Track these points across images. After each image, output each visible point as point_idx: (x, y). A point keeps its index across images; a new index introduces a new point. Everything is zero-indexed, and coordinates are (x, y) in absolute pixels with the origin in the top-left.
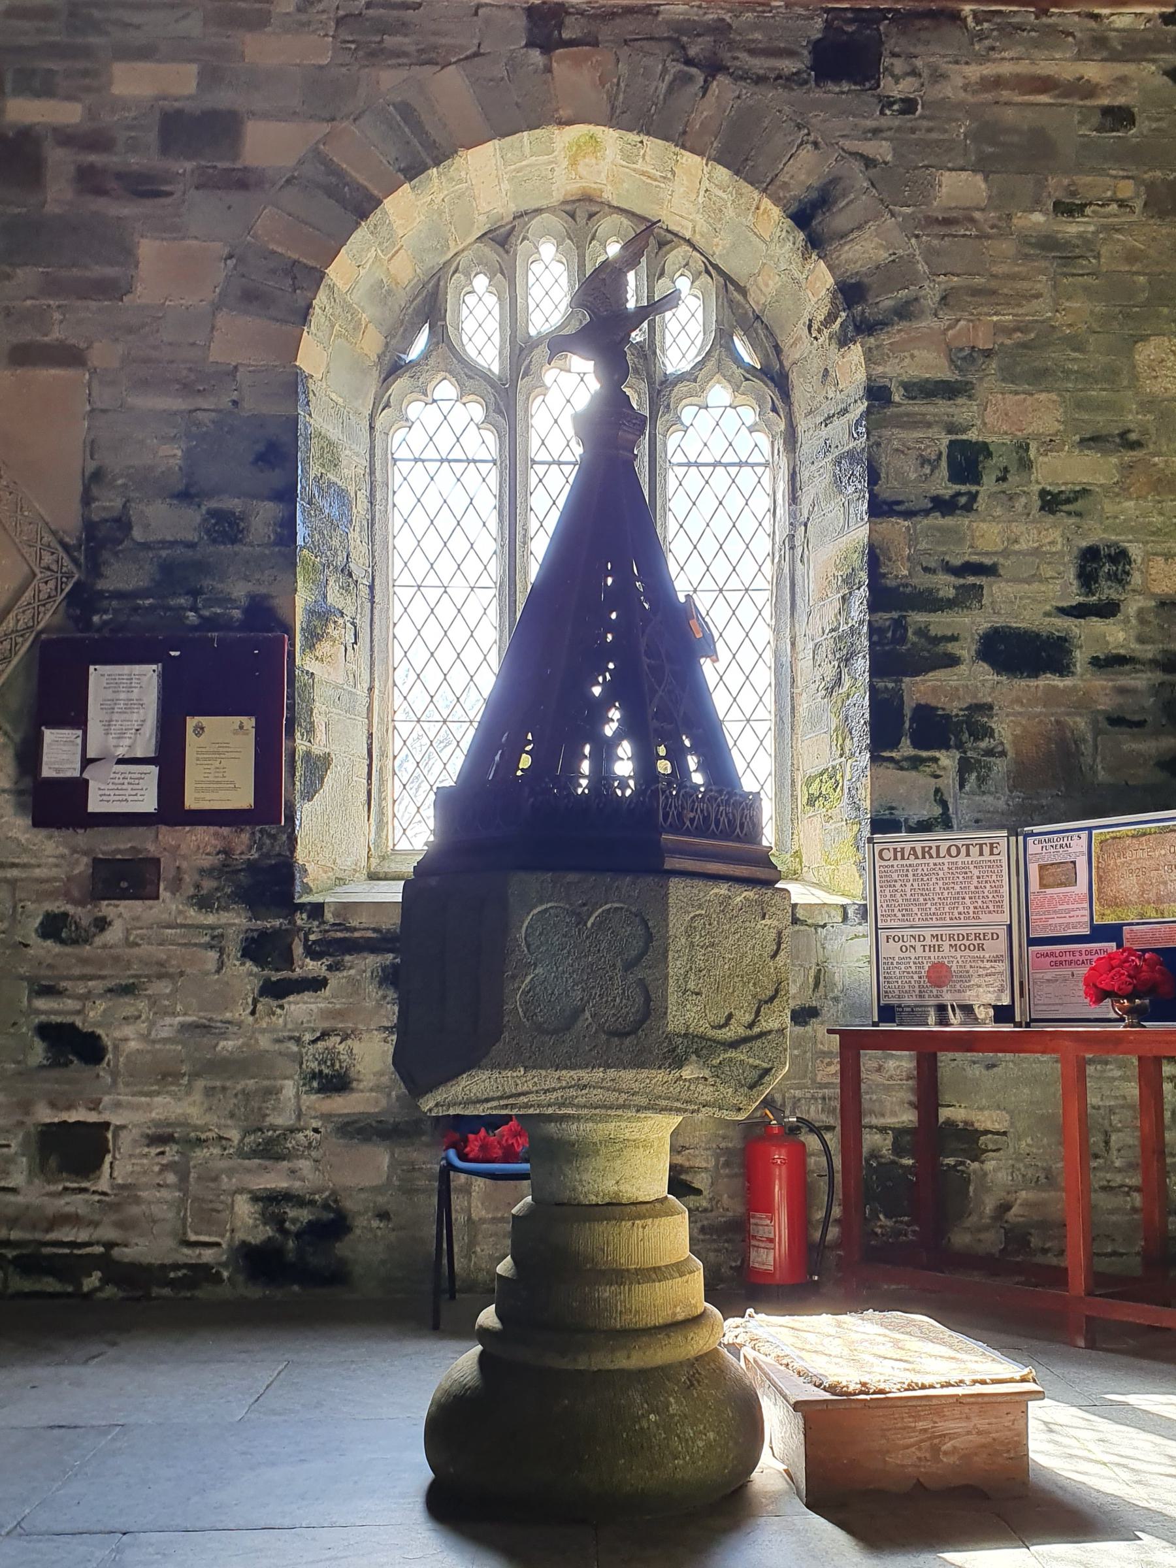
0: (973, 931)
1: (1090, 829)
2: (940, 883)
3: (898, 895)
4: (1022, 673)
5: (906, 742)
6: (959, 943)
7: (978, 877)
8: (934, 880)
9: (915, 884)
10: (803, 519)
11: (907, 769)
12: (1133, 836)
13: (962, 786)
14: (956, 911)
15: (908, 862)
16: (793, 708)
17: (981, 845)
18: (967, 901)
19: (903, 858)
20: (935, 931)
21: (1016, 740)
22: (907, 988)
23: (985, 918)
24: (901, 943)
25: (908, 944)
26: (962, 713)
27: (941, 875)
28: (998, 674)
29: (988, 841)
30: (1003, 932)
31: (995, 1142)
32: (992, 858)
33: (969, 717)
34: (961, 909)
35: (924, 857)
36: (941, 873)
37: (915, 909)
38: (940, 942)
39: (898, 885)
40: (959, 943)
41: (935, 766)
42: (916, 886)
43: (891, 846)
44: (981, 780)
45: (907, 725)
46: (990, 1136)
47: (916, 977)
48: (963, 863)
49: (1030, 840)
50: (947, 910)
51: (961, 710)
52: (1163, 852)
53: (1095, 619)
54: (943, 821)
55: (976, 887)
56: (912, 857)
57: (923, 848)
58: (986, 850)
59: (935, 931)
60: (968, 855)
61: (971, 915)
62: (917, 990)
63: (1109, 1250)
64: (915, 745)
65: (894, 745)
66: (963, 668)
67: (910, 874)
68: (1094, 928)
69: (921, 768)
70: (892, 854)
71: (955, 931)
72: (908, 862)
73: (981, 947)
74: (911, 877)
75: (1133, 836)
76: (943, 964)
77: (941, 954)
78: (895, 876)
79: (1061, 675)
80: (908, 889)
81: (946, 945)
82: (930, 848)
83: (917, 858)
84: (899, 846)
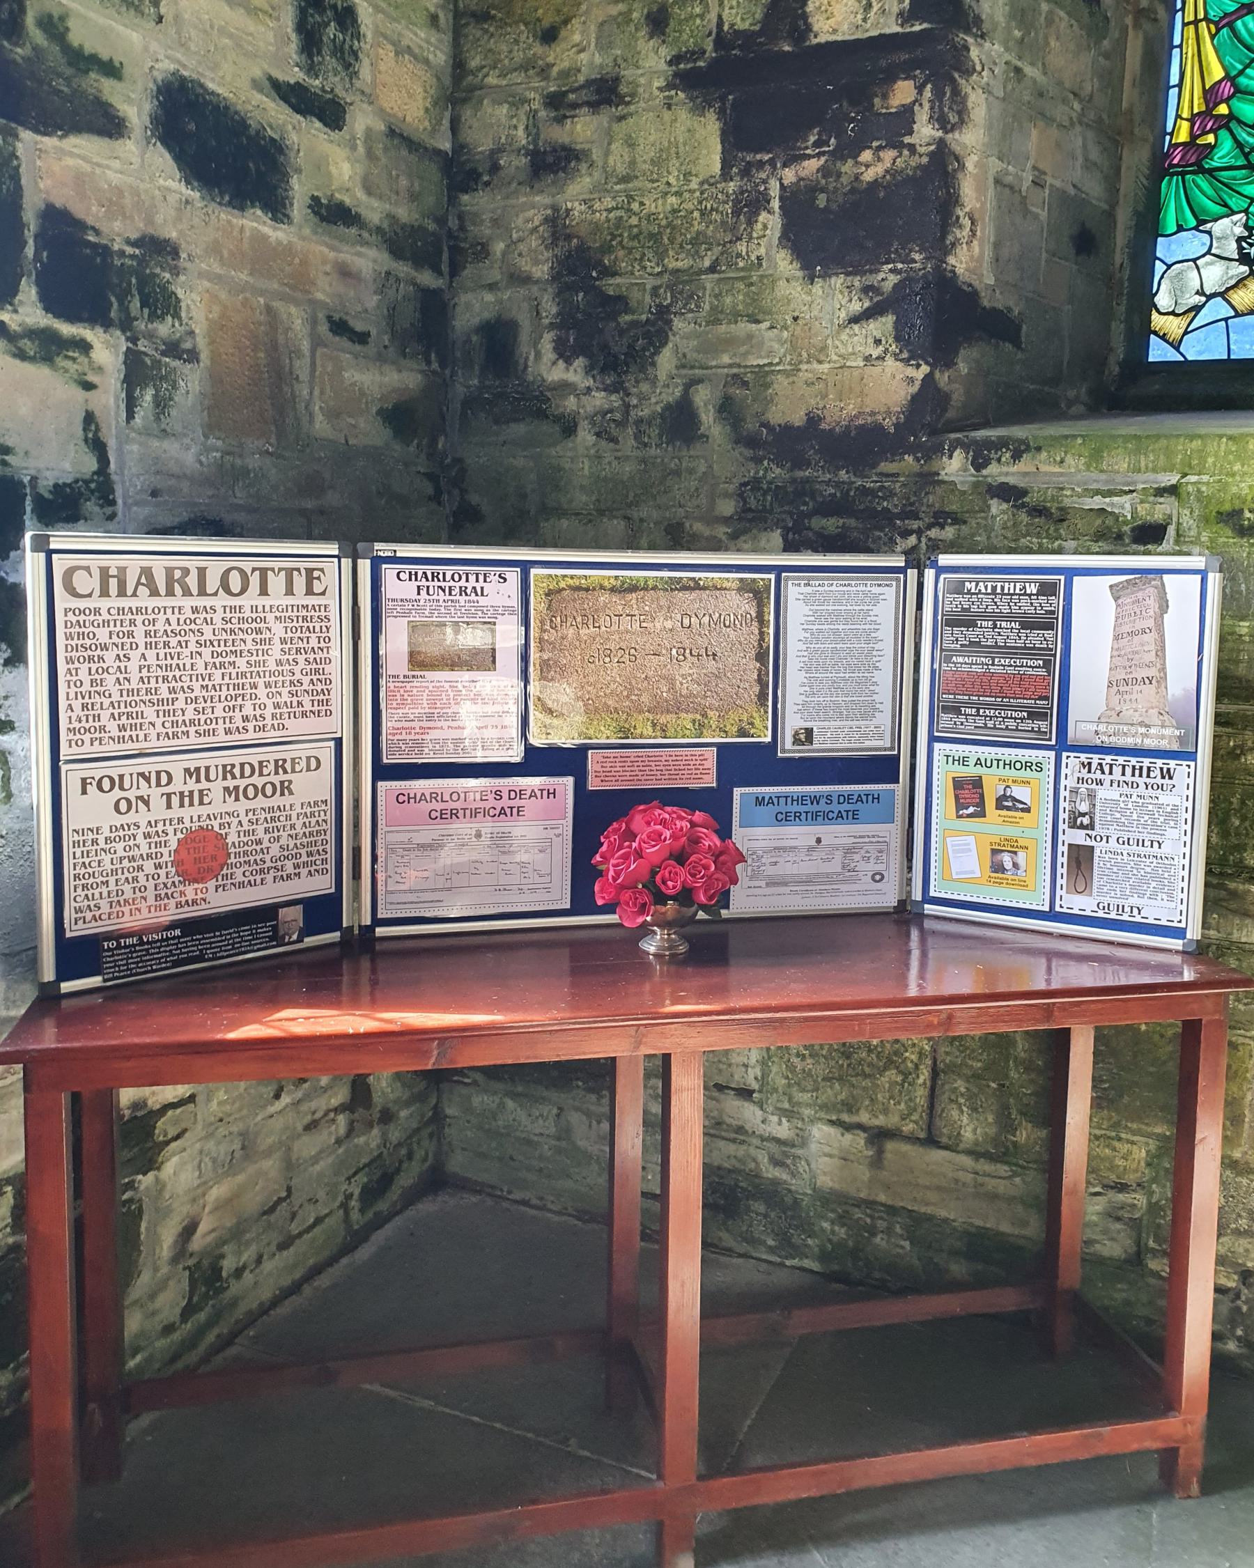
0: (270, 754)
1: (525, 566)
2: (206, 652)
3: (110, 680)
4: (222, 194)
5: (28, 292)
6: (242, 783)
7: (283, 641)
8: (192, 647)
9: (150, 654)
11: (32, 359)
12: (613, 590)
13: (130, 415)
15: (134, 603)
17: (289, 573)
18: (262, 692)
19: (122, 593)
20: (193, 761)
21: (217, 328)
22: (129, 894)
23: (296, 727)
24: (117, 793)
25: (131, 795)
26: (129, 250)
27: (208, 635)
28: (188, 183)
29: (303, 564)
30: (326, 753)
31: (176, 1122)
32: (311, 601)
33: (142, 261)
34: (248, 710)
35: (170, 593)
36: (207, 630)
37: (150, 713)
38: (204, 784)
39: (110, 656)
40: (242, 783)
41: (83, 359)
42: (151, 660)
43: (95, 562)
44: (161, 405)
45: (30, 251)
46: (170, 1113)
47: (149, 866)
48: (254, 609)
49: (389, 571)
50: (219, 712)
51: (128, 242)
52: (669, 624)
53: (318, 124)
54: (98, 489)
55: (279, 663)
56: (144, 591)
57: (169, 571)
58: (300, 582)
59: (193, 761)
60: (264, 592)
61: (269, 721)
62: (150, 894)
63: (312, 1220)
64: (51, 303)
66: (129, 148)
67: (139, 632)
68: (530, 750)
69: (60, 362)
70: (95, 583)
71: (235, 757)
72: (134, 603)
73: (285, 788)
74: (140, 638)
75: (613, 590)
76: (209, 830)
77: (204, 811)
79: (274, 219)
80: (133, 666)
81: (217, 788)
82: (186, 572)
84: (113, 562)
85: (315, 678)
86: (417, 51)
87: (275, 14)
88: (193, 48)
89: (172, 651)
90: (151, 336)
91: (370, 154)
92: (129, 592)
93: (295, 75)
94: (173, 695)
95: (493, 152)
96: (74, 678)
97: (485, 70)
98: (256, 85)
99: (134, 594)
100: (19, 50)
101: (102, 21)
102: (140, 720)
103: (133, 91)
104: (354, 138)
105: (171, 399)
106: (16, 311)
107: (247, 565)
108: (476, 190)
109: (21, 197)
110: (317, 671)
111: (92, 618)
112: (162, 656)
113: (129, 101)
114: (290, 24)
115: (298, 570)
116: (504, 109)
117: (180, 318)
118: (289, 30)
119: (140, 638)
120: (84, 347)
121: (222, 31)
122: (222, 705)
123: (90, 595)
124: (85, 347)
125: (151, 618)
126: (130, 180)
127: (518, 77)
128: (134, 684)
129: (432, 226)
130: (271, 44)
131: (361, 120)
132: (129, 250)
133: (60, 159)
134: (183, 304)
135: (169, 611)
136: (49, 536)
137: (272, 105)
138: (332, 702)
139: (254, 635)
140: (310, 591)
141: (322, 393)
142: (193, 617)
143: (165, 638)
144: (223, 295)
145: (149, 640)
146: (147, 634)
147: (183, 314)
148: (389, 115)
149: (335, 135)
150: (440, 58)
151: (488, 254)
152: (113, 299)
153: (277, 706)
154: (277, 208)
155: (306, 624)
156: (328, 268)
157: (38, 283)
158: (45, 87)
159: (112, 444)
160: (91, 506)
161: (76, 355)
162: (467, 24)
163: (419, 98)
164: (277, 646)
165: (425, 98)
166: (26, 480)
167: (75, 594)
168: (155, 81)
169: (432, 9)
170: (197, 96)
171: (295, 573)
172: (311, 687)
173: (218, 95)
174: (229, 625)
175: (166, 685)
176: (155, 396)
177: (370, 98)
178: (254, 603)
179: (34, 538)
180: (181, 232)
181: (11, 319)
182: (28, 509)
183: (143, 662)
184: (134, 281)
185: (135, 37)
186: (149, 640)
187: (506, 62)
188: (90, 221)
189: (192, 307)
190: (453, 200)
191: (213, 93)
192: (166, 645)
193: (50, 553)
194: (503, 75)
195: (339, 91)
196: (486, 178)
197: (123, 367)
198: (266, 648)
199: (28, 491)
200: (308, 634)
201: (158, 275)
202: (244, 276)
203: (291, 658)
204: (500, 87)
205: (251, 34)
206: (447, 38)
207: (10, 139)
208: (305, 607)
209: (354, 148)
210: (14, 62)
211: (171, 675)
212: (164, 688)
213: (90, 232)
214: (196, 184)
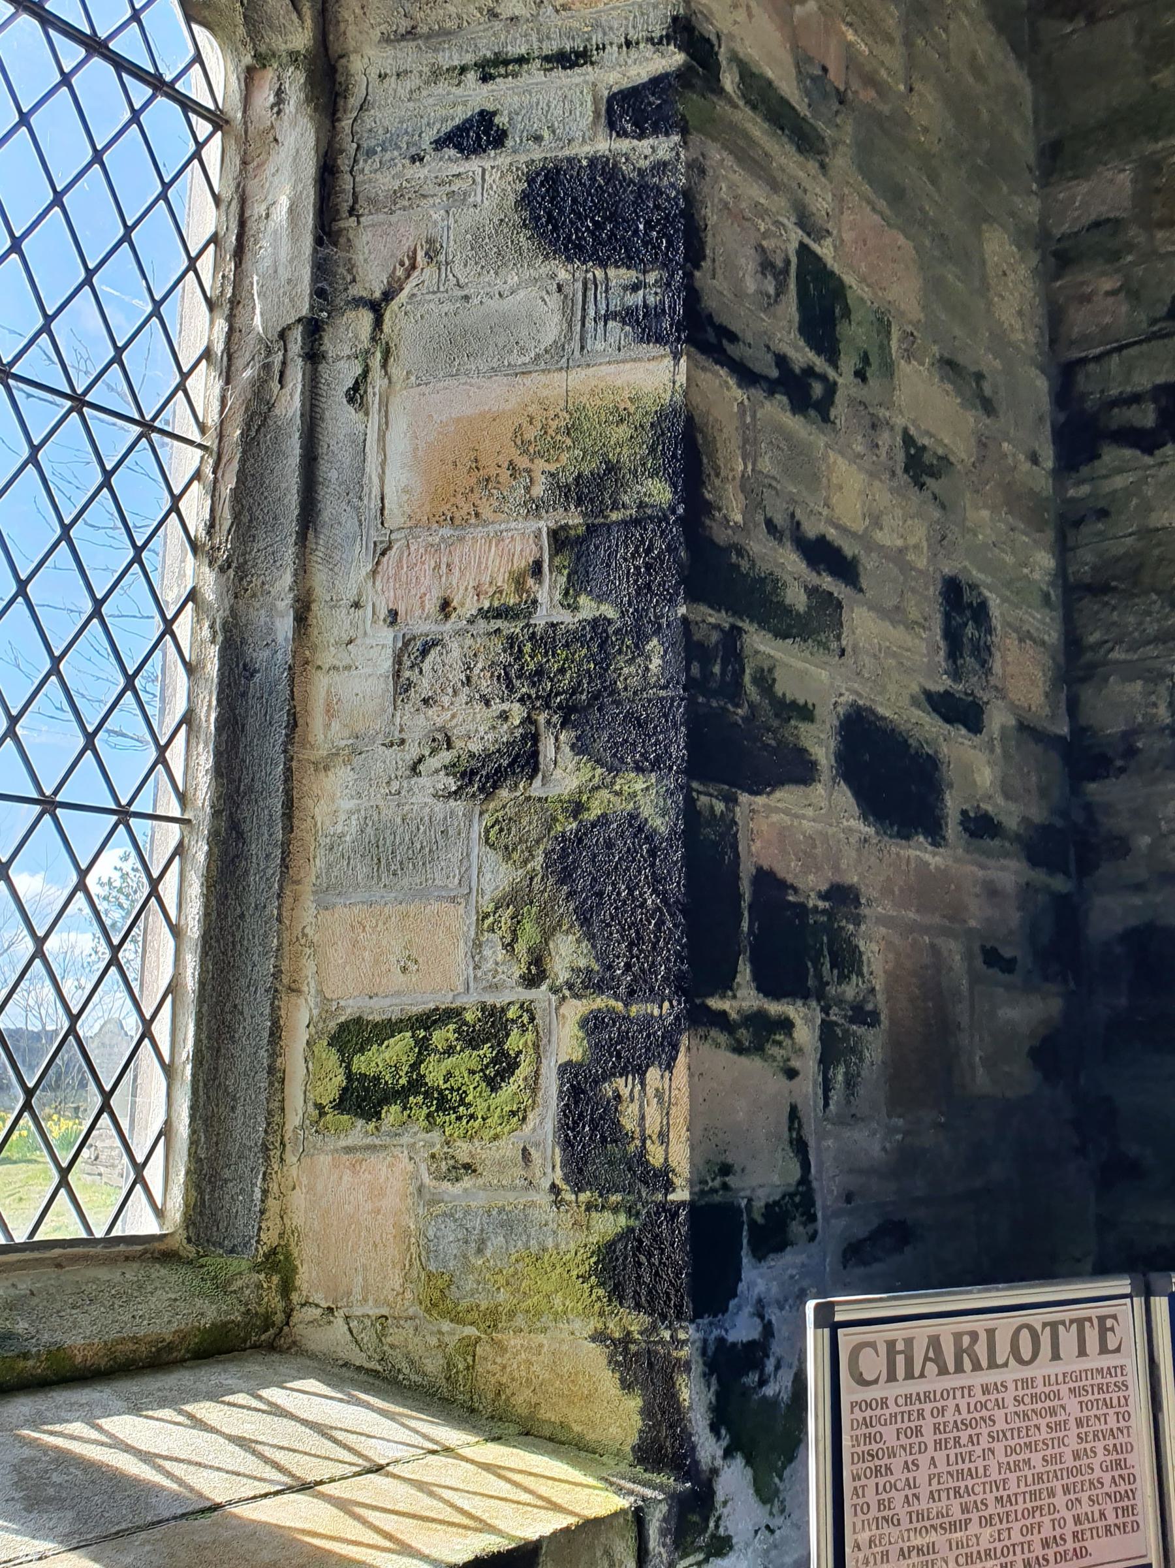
2: (999, 1447)
9: (940, 1456)
10: (373, 282)
14: (1036, 1538)
16: (289, 805)
17: (1080, 1322)
18: (1060, 1500)
19: (909, 1375)
21: (893, 978)
26: (822, 905)
27: (1001, 1425)
35: (959, 1369)
36: (999, 1415)
45: (745, 925)
48: (1046, 1380)
53: (963, 731)
55: (1076, 1456)
56: (932, 1368)
57: (958, 1337)
64: (768, 986)
65: (725, 985)
74: (929, 1437)
78: (889, 1432)
79: (935, 844)
80: (922, 1476)
82: (974, 1336)
83: (943, 1371)
85: (1116, 1474)
86: (1035, 635)
87: (927, 624)
88: (866, 675)
89: (963, 1450)
90: (840, 1002)
91: (1006, 755)
92: (917, 1373)
93: (943, 683)
94: (966, 1516)
95: (1126, 735)
96: (860, 1501)
97: (1110, 645)
98: (915, 702)
99: (922, 1375)
100: (740, 711)
101: (800, 665)
102: (932, 1557)
103: (822, 731)
104: (992, 739)
105: (859, 1075)
106: (734, 997)
107: (1036, 1318)
108: (1107, 777)
109: (739, 865)
110: (1118, 1463)
111: (878, 1412)
112: (952, 1459)
113: (820, 742)
114: (938, 631)
115: (1090, 1319)
116: (1139, 685)
117: (863, 976)
118: (938, 638)
119: (929, 1437)
120: (786, 1025)
121: (890, 653)
122: (1020, 1524)
123: (876, 1381)
124: (786, 1025)
125: (939, 1405)
126: (819, 826)
127: (1151, 650)
128: (924, 1505)
129: (1059, 823)
130: (925, 656)
131: (998, 719)
132: (822, 905)
133: (767, 817)
134: (864, 958)
135: (958, 1394)
136: (832, 1304)
137: (928, 719)
138: (1139, 1509)
139: (1048, 1419)
140: (1104, 1350)
141: (982, 1040)
142: (983, 1399)
143: (955, 1433)
144: (897, 941)
145: (938, 1437)
146: (936, 1428)
147: (865, 970)
148: (1017, 707)
149: (977, 739)
150: (1053, 636)
151: (1128, 851)
152: (809, 964)
153: (1077, 1520)
154: (934, 832)
155: (1102, 1396)
156: (977, 890)
157: (752, 961)
158: (759, 744)
159: (812, 1142)
160: (796, 1228)
161: (782, 1037)
162: (1080, 599)
163: (1040, 684)
164: (1074, 1430)
165: (1045, 682)
166: (743, 1203)
167: (862, 1382)
168: (838, 717)
169: (1045, 587)
170: (870, 723)
171: (1087, 1324)
172: (1114, 1488)
173: (886, 718)
174: (1022, 1407)
175: (959, 1500)
176: (846, 1074)
177: (1001, 692)
178: (1046, 1372)
179: (818, 1308)
180: (862, 877)
181: (731, 1007)
182: (745, 1241)
183: (933, 1471)
184: (825, 938)
185: (824, 675)
186: (938, 1437)
187: (1136, 634)
188: (790, 879)
189: (872, 959)
190: (1075, 790)
191: (884, 718)
192: (957, 1441)
193: (835, 1327)
194: (1132, 648)
195: (979, 693)
196: (1119, 763)
197: (819, 1044)
198: (1061, 1434)
199: (745, 1218)
200: (1105, 1411)
201: (843, 928)
202: (912, 915)
203: (1088, 1446)
204: (1130, 661)
205: (908, 650)
206: (1058, 614)
207: (731, 805)
208: (1100, 1371)
209: (992, 751)
210: (736, 724)
211: (962, 1484)
212: (956, 1504)
213: (790, 891)
214: (871, 819)
